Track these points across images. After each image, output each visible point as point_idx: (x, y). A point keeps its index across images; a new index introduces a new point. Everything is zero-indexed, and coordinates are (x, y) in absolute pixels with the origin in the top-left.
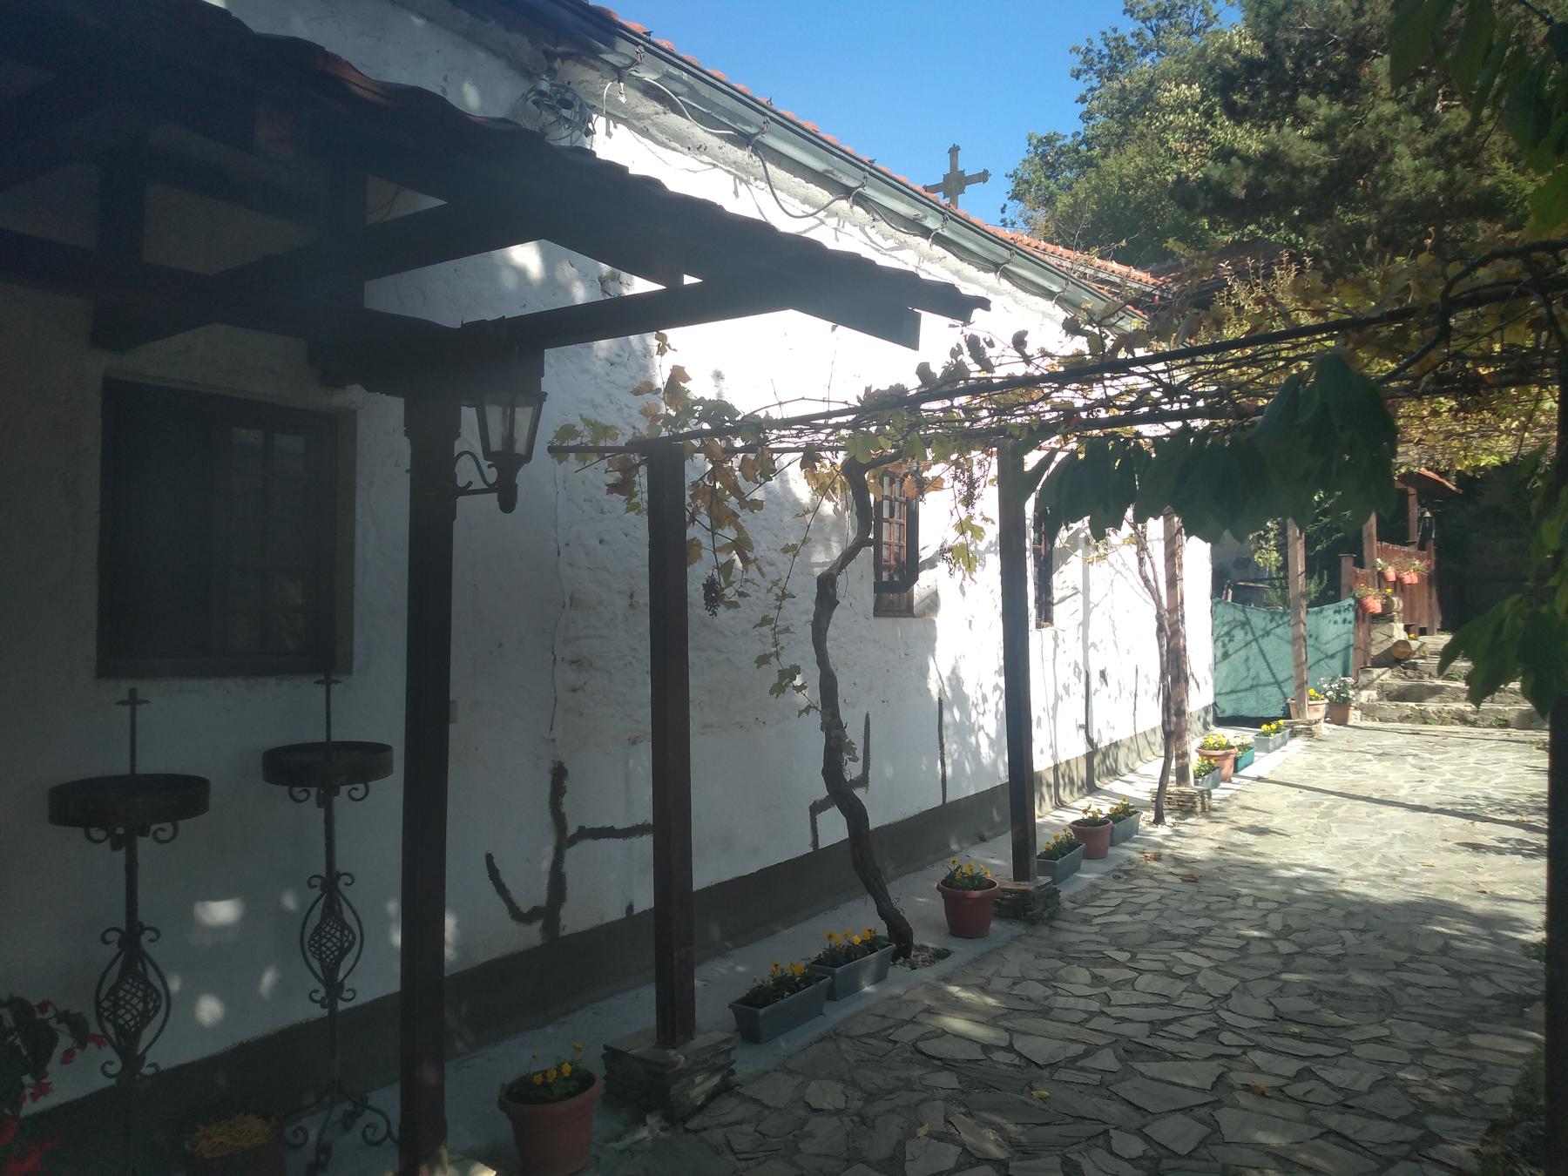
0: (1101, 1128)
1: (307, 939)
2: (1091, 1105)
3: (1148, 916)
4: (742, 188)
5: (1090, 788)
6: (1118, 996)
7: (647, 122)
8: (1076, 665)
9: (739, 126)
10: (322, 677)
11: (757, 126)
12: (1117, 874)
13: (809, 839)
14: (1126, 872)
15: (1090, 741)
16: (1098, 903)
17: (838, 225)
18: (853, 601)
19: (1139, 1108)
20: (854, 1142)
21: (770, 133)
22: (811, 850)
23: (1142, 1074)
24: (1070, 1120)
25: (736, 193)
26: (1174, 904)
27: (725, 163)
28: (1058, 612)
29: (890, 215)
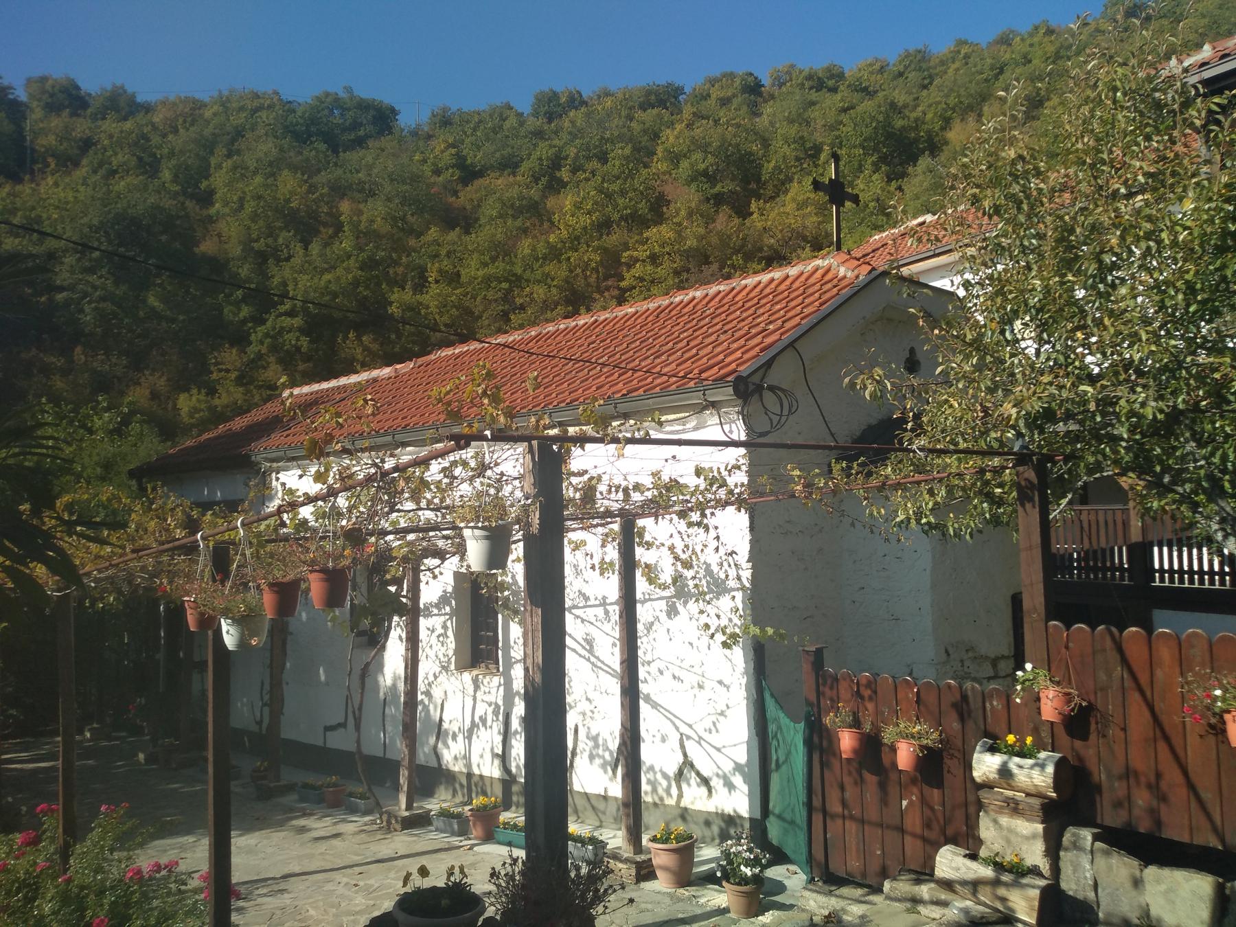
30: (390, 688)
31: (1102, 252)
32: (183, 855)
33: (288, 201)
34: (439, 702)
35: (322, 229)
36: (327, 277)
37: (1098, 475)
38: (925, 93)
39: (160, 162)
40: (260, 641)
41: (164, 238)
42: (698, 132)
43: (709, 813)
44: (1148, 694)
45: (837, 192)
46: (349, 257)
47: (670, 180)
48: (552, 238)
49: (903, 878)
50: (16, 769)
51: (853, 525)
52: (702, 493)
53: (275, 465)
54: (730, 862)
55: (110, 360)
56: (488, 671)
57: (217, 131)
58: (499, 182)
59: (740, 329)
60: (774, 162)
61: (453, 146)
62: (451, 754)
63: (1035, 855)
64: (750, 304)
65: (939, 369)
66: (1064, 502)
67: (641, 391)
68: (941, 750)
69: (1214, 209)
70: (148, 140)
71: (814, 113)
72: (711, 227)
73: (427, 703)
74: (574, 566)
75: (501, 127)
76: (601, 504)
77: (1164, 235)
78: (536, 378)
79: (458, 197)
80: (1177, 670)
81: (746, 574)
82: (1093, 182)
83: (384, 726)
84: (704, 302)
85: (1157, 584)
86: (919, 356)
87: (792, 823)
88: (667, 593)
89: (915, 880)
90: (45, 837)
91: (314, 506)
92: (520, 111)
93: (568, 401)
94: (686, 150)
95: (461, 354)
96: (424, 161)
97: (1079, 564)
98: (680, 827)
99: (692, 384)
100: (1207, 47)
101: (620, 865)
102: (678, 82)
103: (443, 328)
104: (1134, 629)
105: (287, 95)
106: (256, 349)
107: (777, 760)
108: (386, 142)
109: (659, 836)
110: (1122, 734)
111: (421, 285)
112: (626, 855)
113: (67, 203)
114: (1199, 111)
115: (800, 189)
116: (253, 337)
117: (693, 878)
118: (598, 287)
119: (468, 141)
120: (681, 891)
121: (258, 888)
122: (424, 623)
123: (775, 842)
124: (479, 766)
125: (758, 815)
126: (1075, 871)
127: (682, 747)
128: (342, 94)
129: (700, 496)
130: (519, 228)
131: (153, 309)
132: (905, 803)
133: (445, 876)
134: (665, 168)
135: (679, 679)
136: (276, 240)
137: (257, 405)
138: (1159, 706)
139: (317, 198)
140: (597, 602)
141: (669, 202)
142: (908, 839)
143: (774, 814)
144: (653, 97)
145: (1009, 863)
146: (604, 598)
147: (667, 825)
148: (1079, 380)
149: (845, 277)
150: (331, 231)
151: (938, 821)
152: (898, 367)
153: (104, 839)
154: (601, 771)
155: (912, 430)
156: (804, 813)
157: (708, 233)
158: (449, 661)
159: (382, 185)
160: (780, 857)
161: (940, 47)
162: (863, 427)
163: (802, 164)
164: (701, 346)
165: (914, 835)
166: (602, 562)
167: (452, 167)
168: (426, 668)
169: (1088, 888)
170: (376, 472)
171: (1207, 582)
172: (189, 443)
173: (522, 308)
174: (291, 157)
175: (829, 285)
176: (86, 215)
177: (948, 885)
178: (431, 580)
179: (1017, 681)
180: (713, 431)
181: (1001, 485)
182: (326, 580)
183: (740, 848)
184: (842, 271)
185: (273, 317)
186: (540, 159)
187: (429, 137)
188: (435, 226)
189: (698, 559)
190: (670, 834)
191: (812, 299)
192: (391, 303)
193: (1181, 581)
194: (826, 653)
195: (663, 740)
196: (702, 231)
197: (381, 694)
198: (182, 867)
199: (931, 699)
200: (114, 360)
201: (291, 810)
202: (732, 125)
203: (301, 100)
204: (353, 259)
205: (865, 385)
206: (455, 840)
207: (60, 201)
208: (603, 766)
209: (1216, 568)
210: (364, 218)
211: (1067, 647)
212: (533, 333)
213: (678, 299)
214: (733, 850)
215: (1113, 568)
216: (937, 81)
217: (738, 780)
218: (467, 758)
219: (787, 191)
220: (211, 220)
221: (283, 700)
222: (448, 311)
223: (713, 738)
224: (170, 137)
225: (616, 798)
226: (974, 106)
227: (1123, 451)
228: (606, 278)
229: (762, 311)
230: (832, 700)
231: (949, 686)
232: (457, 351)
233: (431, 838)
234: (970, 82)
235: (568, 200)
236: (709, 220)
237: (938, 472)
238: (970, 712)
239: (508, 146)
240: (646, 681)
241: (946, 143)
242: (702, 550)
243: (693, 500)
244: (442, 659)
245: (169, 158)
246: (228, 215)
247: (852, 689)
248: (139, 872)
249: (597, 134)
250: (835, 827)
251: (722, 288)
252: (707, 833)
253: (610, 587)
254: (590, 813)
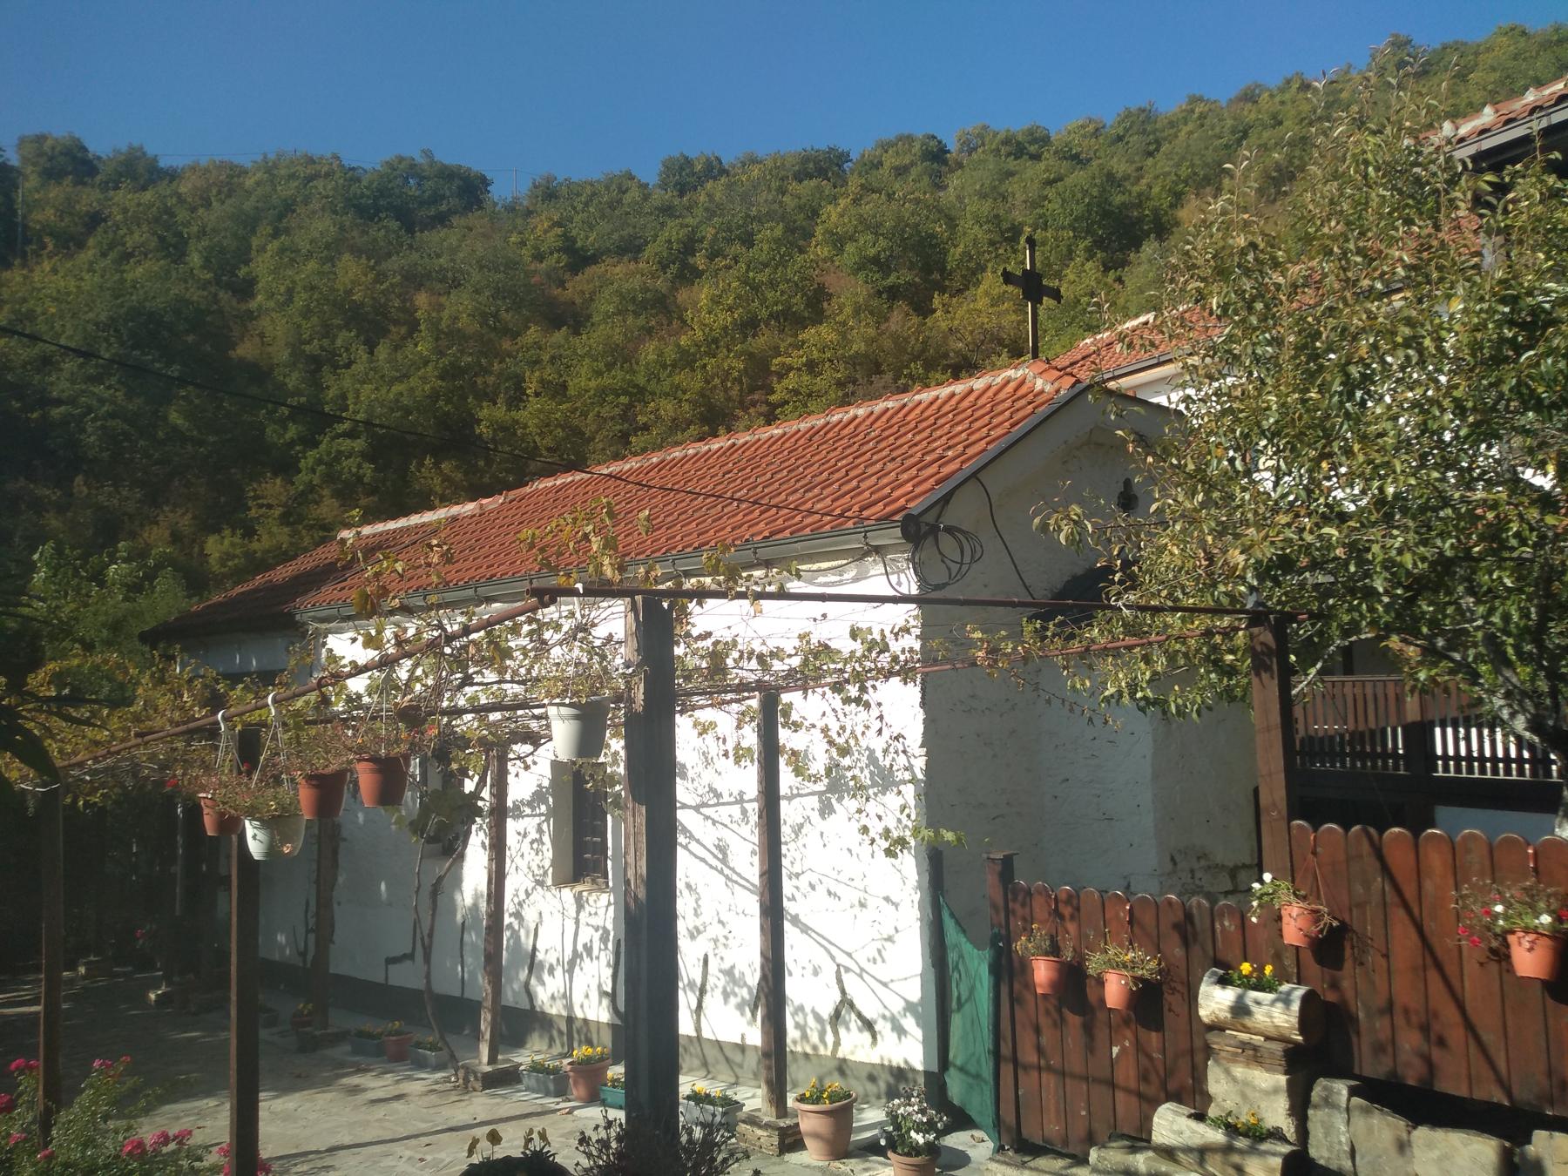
30: (470, 909)
31: (1349, 363)
32: (201, 1124)
33: (349, 292)
34: (533, 926)
35: (392, 328)
36: (397, 388)
37: (1354, 638)
38: (1150, 161)
39: (186, 243)
40: (294, 848)
41: (190, 338)
42: (866, 209)
43: (873, 1065)
44: (1416, 911)
45: (1032, 286)
46: (426, 363)
47: (832, 269)
48: (684, 341)
49: (1114, 1144)
51: (1049, 702)
52: (859, 661)
53: (324, 626)
54: (898, 1127)
55: (119, 493)
56: (595, 887)
57: (260, 205)
58: (618, 269)
59: (911, 456)
60: (962, 246)
61: (559, 224)
62: (547, 994)
63: (1277, 1114)
64: (924, 424)
65: (1154, 507)
66: (1313, 671)
67: (787, 533)
68: (1160, 983)
69: (1487, 312)
70: (172, 215)
71: (1013, 186)
72: (883, 327)
73: (516, 927)
74: (704, 753)
75: (619, 201)
76: (735, 676)
77: (1427, 342)
78: (648, 519)
79: (565, 289)
80: (1451, 882)
81: (920, 764)
82: (1342, 276)
83: (462, 957)
84: (868, 422)
85: (1440, 774)
86: (1136, 491)
87: (978, 1076)
88: (821, 787)
89: (1130, 1147)
90: (20, 1101)
91: (370, 678)
92: (643, 181)
93: (696, 545)
94: (851, 230)
95: (564, 486)
96: (523, 243)
97: (1353, 748)
98: (836, 1083)
99: (850, 524)
100: (1488, 110)
101: (759, 1132)
102: (843, 147)
103: (544, 453)
104: (1396, 830)
105: (349, 160)
106: (306, 479)
107: (959, 998)
108: (475, 219)
109: (808, 1095)
110: (1383, 962)
111: (517, 398)
112: (766, 1119)
113: (68, 294)
114: (1464, 193)
115: (990, 282)
116: (302, 464)
117: (851, 1148)
118: (741, 402)
119: (578, 218)
120: (837, 1164)
121: (296, 1165)
122: (512, 825)
123: (956, 1102)
124: (582, 1006)
125: (935, 1068)
126: (1327, 1135)
127: (840, 981)
128: (420, 159)
129: (857, 665)
130: (643, 328)
131: (175, 428)
132: (1115, 1050)
133: (522, 1143)
134: (826, 253)
135: (835, 895)
136: (333, 342)
137: (306, 550)
138: (1429, 926)
139: (387, 289)
140: (732, 799)
141: (831, 295)
142: (1120, 1096)
143: (955, 1066)
144: (811, 165)
145: (1243, 1124)
146: (741, 793)
147: (821, 1080)
148: (1326, 519)
149: (1042, 392)
150: (403, 330)
151: (1157, 1072)
152: (1108, 503)
153: (96, 1103)
154: (738, 1013)
155: (1121, 582)
156: (991, 1064)
157: (880, 335)
158: (545, 873)
159: (468, 274)
160: (961, 1121)
161: (1169, 105)
162: (1066, 578)
163: (997, 249)
164: (862, 477)
165: (1128, 1091)
166: (738, 747)
167: (558, 251)
168: (514, 884)
169: (1343, 1156)
170: (440, 635)
171: (1501, 772)
172: (217, 598)
173: (646, 428)
174: (353, 238)
175: (1023, 402)
176: (91, 310)
177: (1168, 1153)
178: (522, 772)
179: (1254, 895)
180: (877, 584)
181: (1232, 651)
182: (379, 771)
183: (910, 1109)
184: (1039, 384)
185: (327, 439)
186: (669, 241)
187: (529, 213)
188: (536, 324)
189: (857, 743)
190: (822, 1092)
191: (1000, 418)
192: (479, 421)
193: (1470, 770)
194: (1018, 864)
195: (816, 972)
196: (871, 332)
197: (459, 918)
198: (197, 1139)
199: (1148, 918)
200: (125, 493)
201: (342, 1065)
202: (910, 201)
203: (368, 167)
204: (430, 368)
205: (1059, 527)
206: (550, 1102)
207: (59, 291)
208: (740, 1007)
209: (1513, 754)
210: (445, 314)
211: (1314, 853)
212: (655, 460)
213: (835, 418)
214: (901, 1111)
215: (1385, 755)
216: (1165, 148)
217: (909, 1023)
218: (567, 997)
219: (979, 282)
220: (251, 316)
221: (332, 926)
222: (551, 432)
223: (879, 971)
224: (201, 211)
225: (756, 1047)
226: (1211, 180)
227: (1381, 609)
228: (752, 390)
229: (939, 433)
230: (1024, 919)
231: (1170, 902)
232: (558, 482)
233: (521, 1099)
234: (1207, 148)
235: (703, 293)
236: (882, 318)
237: (1157, 634)
238: (1195, 935)
239: (629, 225)
240: (793, 898)
241: (1177, 224)
242: (863, 733)
243: (849, 668)
244: (536, 872)
245: (199, 239)
246: (273, 310)
247: (1050, 906)
248: (140, 1144)
249: (740, 211)
250: (1028, 1081)
251: (890, 404)
252: (871, 1088)
253: (747, 779)
254: (723, 1066)
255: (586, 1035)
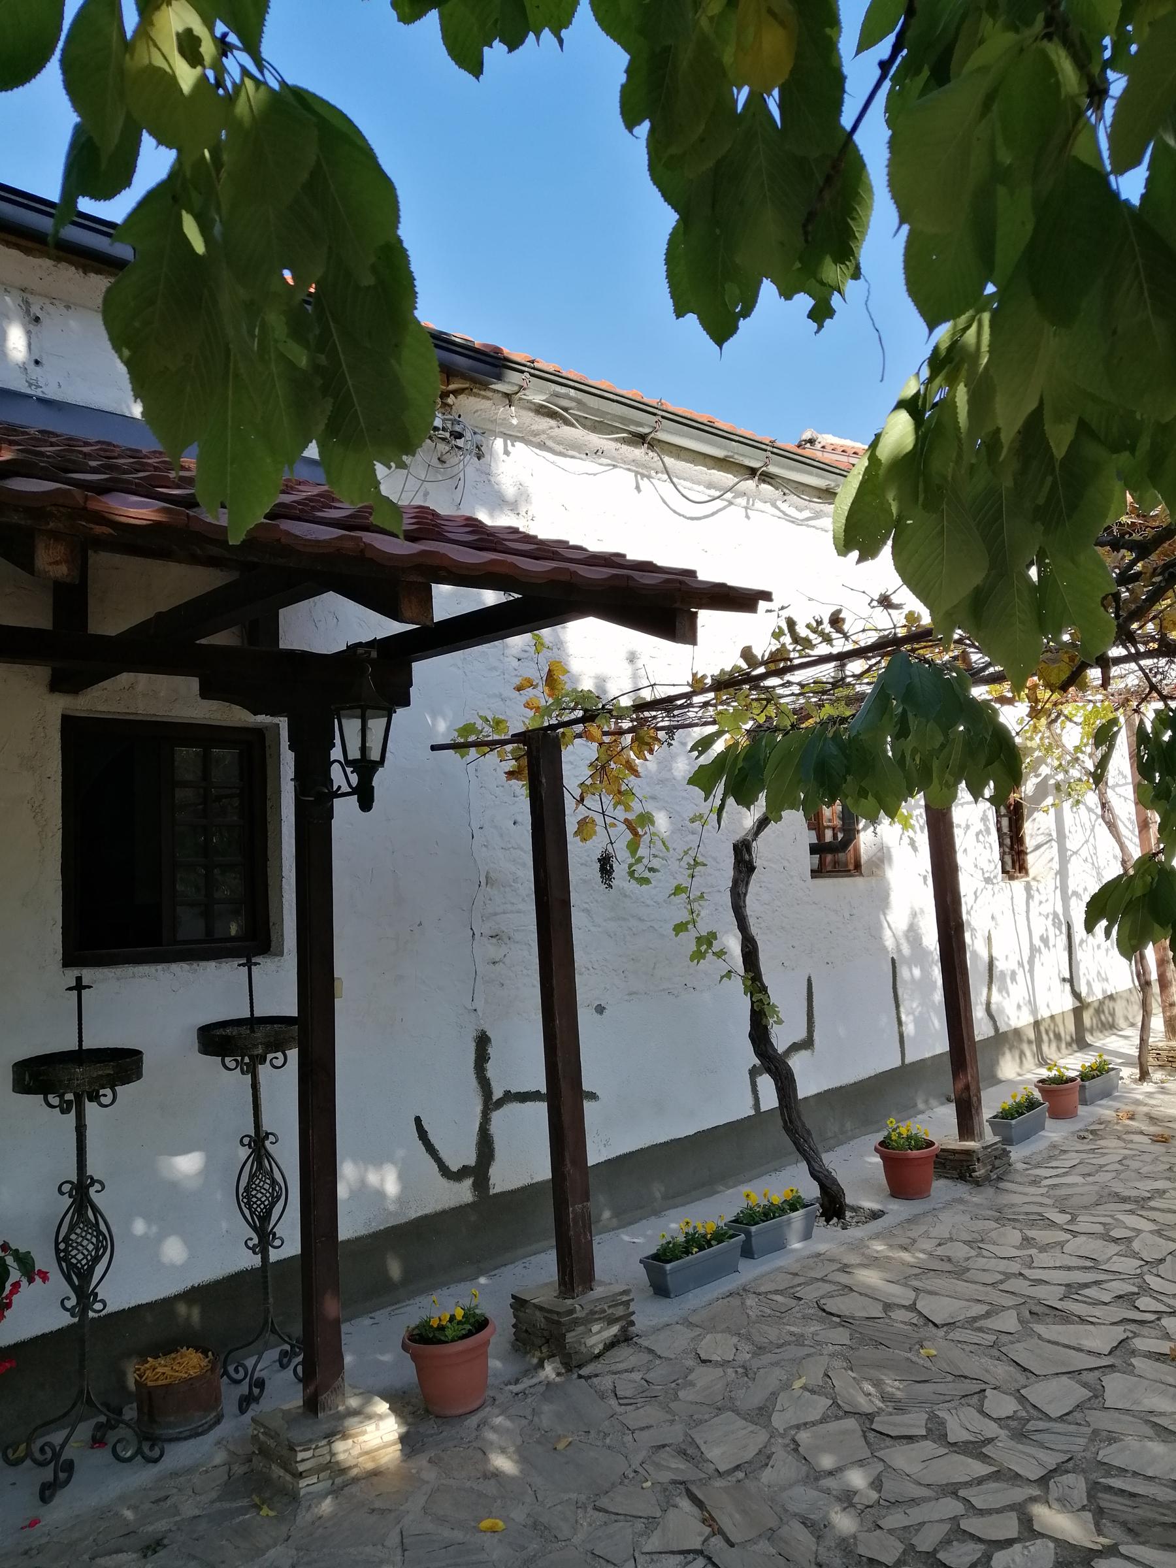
0: (977, 1387)
1: (241, 1191)
2: (974, 1365)
3: (1102, 1177)
4: (644, 484)
5: (1080, 1043)
6: (1043, 1259)
7: (543, 437)
8: (1055, 915)
9: (633, 428)
10: (244, 961)
11: (650, 426)
12: (1082, 1134)
13: (750, 1101)
14: (1093, 1132)
15: (1076, 995)
16: (1054, 1164)
17: (748, 503)
18: (786, 864)
19: (1025, 1370)
20: (730, 1392)
21: (663, 430)
22: (752, 1112)
23: (1040, 1337)
24: (950, 1378)
25: (638, 488)
26: (1134, 1165)
27: (625, 462)
28: (1032, 860)
29: (802, 488)
50: (162, 493)
255: (1054, 1032)
